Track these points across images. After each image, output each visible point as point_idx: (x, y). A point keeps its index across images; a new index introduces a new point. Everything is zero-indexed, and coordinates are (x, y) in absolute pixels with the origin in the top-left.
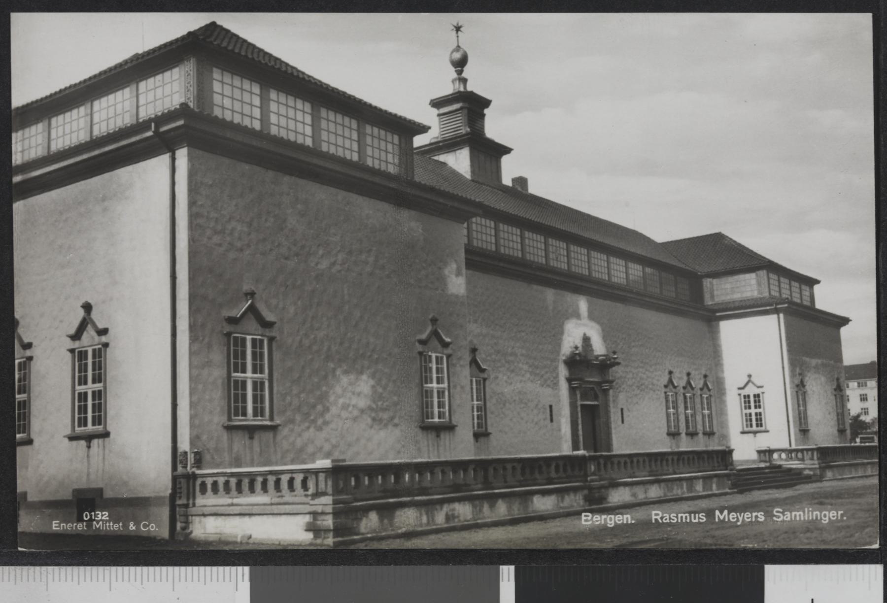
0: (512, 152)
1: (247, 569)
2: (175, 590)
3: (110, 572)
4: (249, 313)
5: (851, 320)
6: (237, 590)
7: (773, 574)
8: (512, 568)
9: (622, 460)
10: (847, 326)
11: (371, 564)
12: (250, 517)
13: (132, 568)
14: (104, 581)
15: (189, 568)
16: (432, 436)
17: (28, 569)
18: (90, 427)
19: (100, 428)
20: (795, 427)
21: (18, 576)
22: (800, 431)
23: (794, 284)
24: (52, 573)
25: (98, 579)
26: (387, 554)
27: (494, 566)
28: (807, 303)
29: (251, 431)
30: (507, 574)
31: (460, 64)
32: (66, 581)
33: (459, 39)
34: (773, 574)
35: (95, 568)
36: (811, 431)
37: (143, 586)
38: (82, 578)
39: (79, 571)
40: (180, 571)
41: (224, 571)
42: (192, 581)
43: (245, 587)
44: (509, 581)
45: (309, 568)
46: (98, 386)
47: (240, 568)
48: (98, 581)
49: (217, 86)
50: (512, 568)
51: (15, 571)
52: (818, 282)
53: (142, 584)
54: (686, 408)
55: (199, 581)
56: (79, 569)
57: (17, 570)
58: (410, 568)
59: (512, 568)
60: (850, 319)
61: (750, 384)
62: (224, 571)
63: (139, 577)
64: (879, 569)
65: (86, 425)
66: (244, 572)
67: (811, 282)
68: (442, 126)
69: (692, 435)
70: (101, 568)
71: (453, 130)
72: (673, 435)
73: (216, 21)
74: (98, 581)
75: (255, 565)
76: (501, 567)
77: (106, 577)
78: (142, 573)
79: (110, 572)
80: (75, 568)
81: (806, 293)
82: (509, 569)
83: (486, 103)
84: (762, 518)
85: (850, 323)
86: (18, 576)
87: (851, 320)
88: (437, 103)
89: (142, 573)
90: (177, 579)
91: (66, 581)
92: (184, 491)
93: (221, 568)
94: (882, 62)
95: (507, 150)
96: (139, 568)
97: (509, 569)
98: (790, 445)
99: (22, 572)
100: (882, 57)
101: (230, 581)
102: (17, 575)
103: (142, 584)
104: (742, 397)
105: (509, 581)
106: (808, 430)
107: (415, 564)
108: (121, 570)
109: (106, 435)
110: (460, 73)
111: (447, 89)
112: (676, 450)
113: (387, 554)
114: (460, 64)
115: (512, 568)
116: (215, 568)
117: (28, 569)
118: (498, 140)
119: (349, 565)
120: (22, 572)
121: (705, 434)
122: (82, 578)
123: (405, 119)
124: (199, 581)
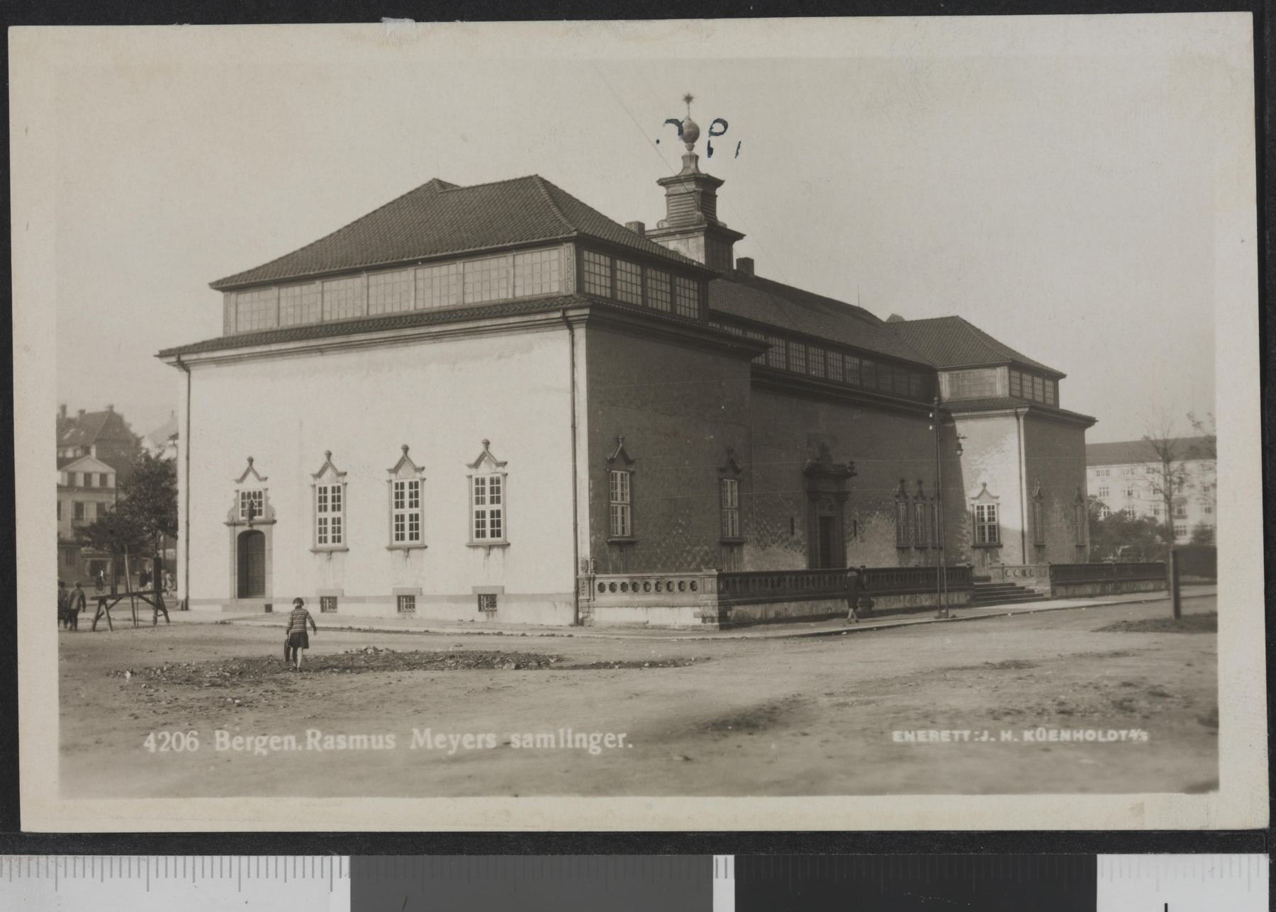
0: (745, 238)
1: (346, 859)
2: (242, 890)
3: (148, 863)
4: (30, 822)
5: (1097, 421)
6: (331, 891)
7: (1107, 863)
8: (731, 858)
10: (1092, 427)
11: (526, 853)
12: (474, 549)
13: (180, 859)
14: (139, 877)
15: (263, 858)
17: (29, 860)
20: (1030, 542)
21: (15, 869)
22: (1036, 546)
24: (63, 866)
25: (130, 874)
26: (549, 838)
27: (703, 857)
28: (1050, 401)
30: (724, 869)
32: (84, 876)
33: (691, 110)
34: (1107, 863)
35: (125, 858)
36: (1047, 546)
37: (195, 884)
38: (107, 873)
39: (102, 862)
40: (249, 861)
41: (313, 862)
42: (267, 876)
43: (343, 886)
44: (726, 877)
45: (437, 858)
47: (336, 858)
48: (130, 877)
50: (731, 858)
51: (11, 861)
53: (194, 882)
55: (276, 876)
56: (102, 858)
57: (13, 860)
58: (584, 858)
59: (731, 858)
60: (1097, 419)
61: (985, 495)
62: (313, 862)
63: (189, 869)
64: (1261, 862)
66: (342, 863)
67: (1055, 377)
68: (671, 208)
69: (921, 549)
70: (134, 858)
71: (678, 215)
72: (902, 549)
73: (896, 313)
74: (130, 877)
75: (358, 853)
76: (715, 857)
77: (141, 871)
78: (194, 865)
79: (148, 863)
80: (98, 858)
81: (1049, 389)
82: (726, 860)
84: (763, 339)
85: (1096, 423)
86: (15, 869)
87: (1097, 421)
89: (194, 865)
90: (244, 874)
91: (84, 876)
93: (309, 858)
94: (1268, 126)
95: (1063, 376)
96: (189, 858)
97: (726, 860)
98: (1024, 563)
99: (20, 864)
100: (1267, 119)
101: (322, 877)
102: (13, 867)
103: (194, 882)
104: (976, 508)
105: (726, 877)
106: (1044, 546)
107: (590, 853)
108: (164, 861)
110: (691, 148)
111: (675, 168)
112: (905, 566)
113: (549, 838)
115: (731, 858)
116: (299, 858)
117: (29, 860)
118: (731, 226)
119: (494, 854)
120: (20, 864)
121: (934, 548)
122: (107, 873)
124: (276, 876)
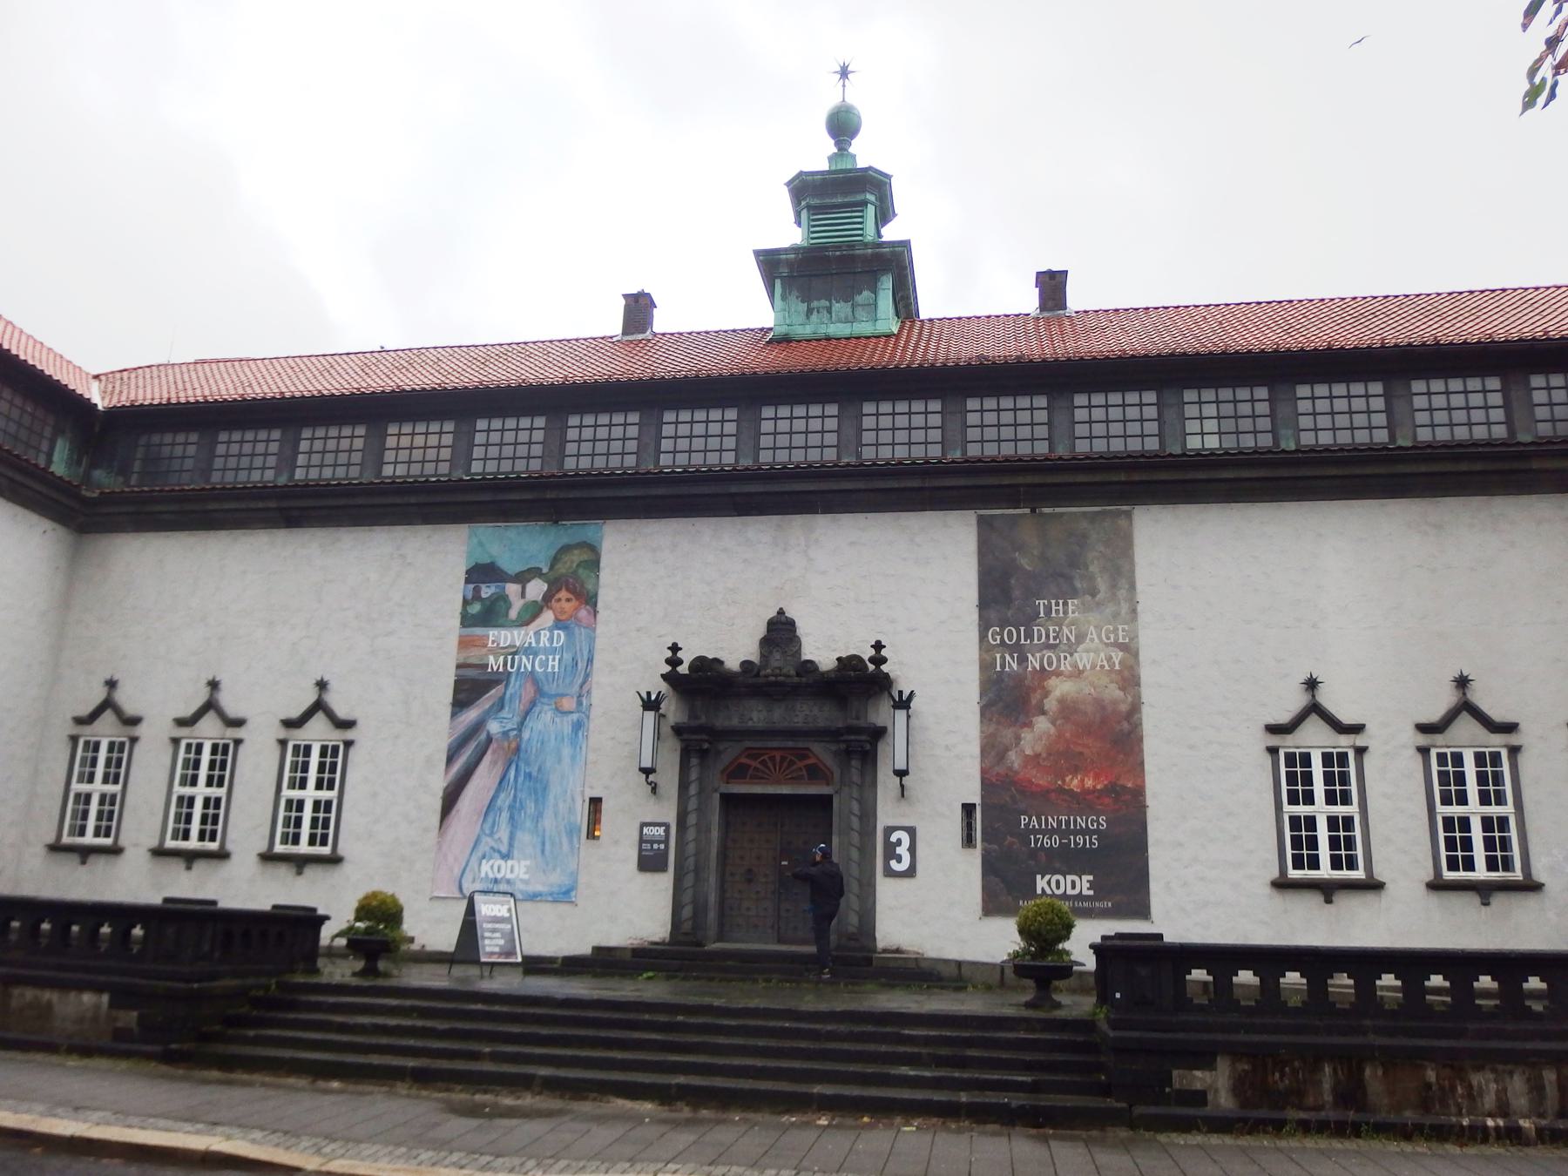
31: (842, 126)
114: (842, 126)
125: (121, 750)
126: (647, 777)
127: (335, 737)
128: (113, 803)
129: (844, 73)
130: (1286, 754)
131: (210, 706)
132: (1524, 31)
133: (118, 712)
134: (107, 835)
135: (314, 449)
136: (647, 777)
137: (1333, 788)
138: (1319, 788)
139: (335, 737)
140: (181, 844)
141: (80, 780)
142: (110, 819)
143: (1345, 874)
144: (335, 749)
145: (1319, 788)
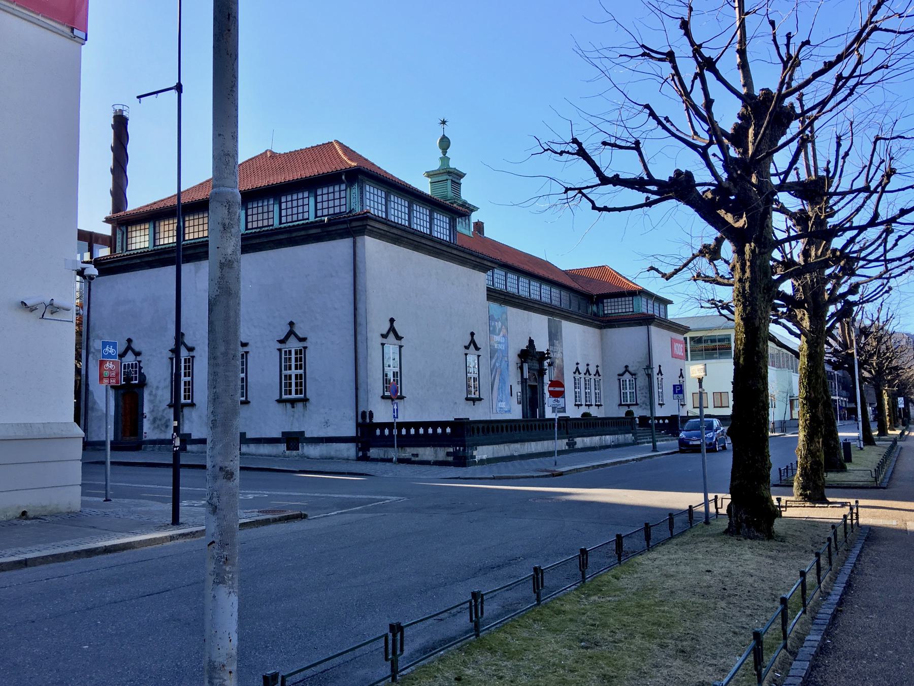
9: (504, 425)
16: (577, 407)
18: (293, 396)
19: (189, 401)
23: (650, 302)
29: (293, 402)
31: (445, 143)
46: (188, 379)
49: (162, 243)
52: (671, 302)
54: (595, 389)
65: (290, 394)
81: (662, 310)
83: (461, 175)
88: (429, 175)
92: (782, 472)
109: (305, 400)
111: (436, 165)
114: (445, 143)
123: (253, 252)
125: (301, 354)
126: (136, 358)
127: (300, 345)
128: (301, 378)
129: (444, 122)
130: (536, 386)
131: (291, 333)
132: (530, 338)
133: (296, 336)
134: (301, 393)
135: (293, 199)
136: (136, 358)
137: (395, 424)
138: (293, 388)
139: (300, 345)
140: (288, 397)
141: (286, 369)
142: (301, 386)
143: (299, 396)
144: (301, 350)
145: (293, 388)
